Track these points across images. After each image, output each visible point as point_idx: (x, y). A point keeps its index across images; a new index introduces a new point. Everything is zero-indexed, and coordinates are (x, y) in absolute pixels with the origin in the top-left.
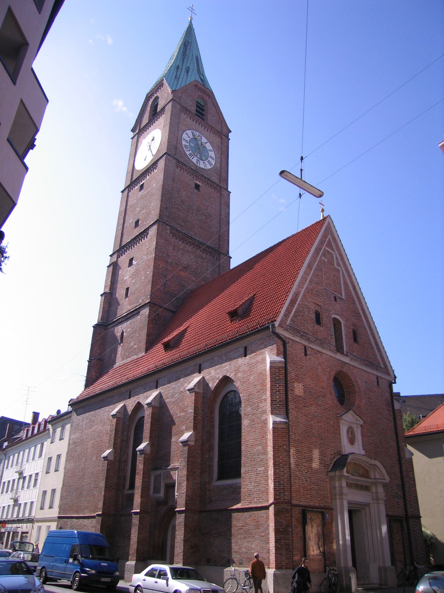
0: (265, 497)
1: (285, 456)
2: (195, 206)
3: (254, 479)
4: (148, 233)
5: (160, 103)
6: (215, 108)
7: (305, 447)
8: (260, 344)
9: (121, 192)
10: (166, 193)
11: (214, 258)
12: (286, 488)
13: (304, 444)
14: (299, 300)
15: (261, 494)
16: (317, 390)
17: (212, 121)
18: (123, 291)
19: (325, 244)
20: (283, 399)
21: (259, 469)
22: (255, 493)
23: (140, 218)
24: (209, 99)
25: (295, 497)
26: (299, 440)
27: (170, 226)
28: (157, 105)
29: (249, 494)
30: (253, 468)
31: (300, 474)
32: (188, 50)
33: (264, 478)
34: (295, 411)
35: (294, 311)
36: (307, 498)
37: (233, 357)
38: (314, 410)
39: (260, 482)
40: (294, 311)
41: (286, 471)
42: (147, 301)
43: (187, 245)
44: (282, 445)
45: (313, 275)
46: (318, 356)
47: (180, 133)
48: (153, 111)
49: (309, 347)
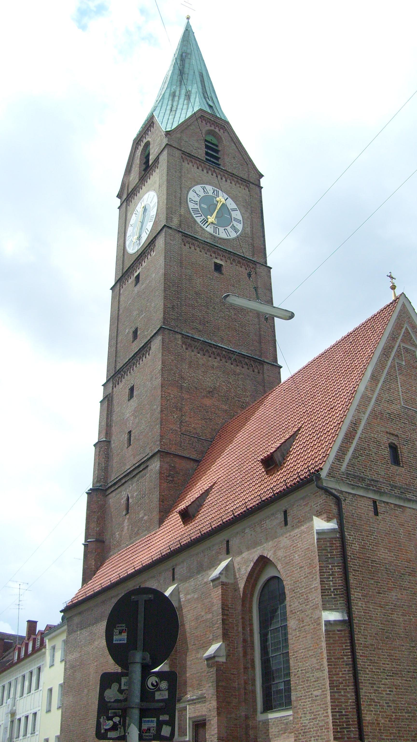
0: (325, 735)
1: (347, 672)
2: (217, 297)
3: (308, 709)
4: (150, 347)
5: (151, 152)
6: (235, 145)
7: (384, 655)
8: (304, 505)
9: (111, 289)
10: (171, 285)
11: (254, 371)
12: (350, 720)
13: (381, 651)
14: (359, 432)
15: (320, 731)
16: (398, 566)
17: (232, 166)
18: (125, 437)
19: (400, 338)
20: (339, 586)
21: (316, 693)
22: (312, 730)
23: (139, 325)
24: (224, 133)
25: (371, 732)
26: (373, 645)
27: (180, 333)
28: (149, 155)
29: (303, 733)
30: (307, 692)
31: (377, 696)
32: (187, 66)
33: (322, 706)
34: (362, 601)
35: (351, 450)
36: (393, 733)
37: (270, 527)
38: (396, 596)
39: (317, 713)
40: (351, 450)
41: (349, 695)
42: (157, 450)
43: (210, 358)
44: (341, 655)
45: (381, 389)
46: (397, 512)
47: (184, 191)
48: (144, 164)
49: (381, 501)
